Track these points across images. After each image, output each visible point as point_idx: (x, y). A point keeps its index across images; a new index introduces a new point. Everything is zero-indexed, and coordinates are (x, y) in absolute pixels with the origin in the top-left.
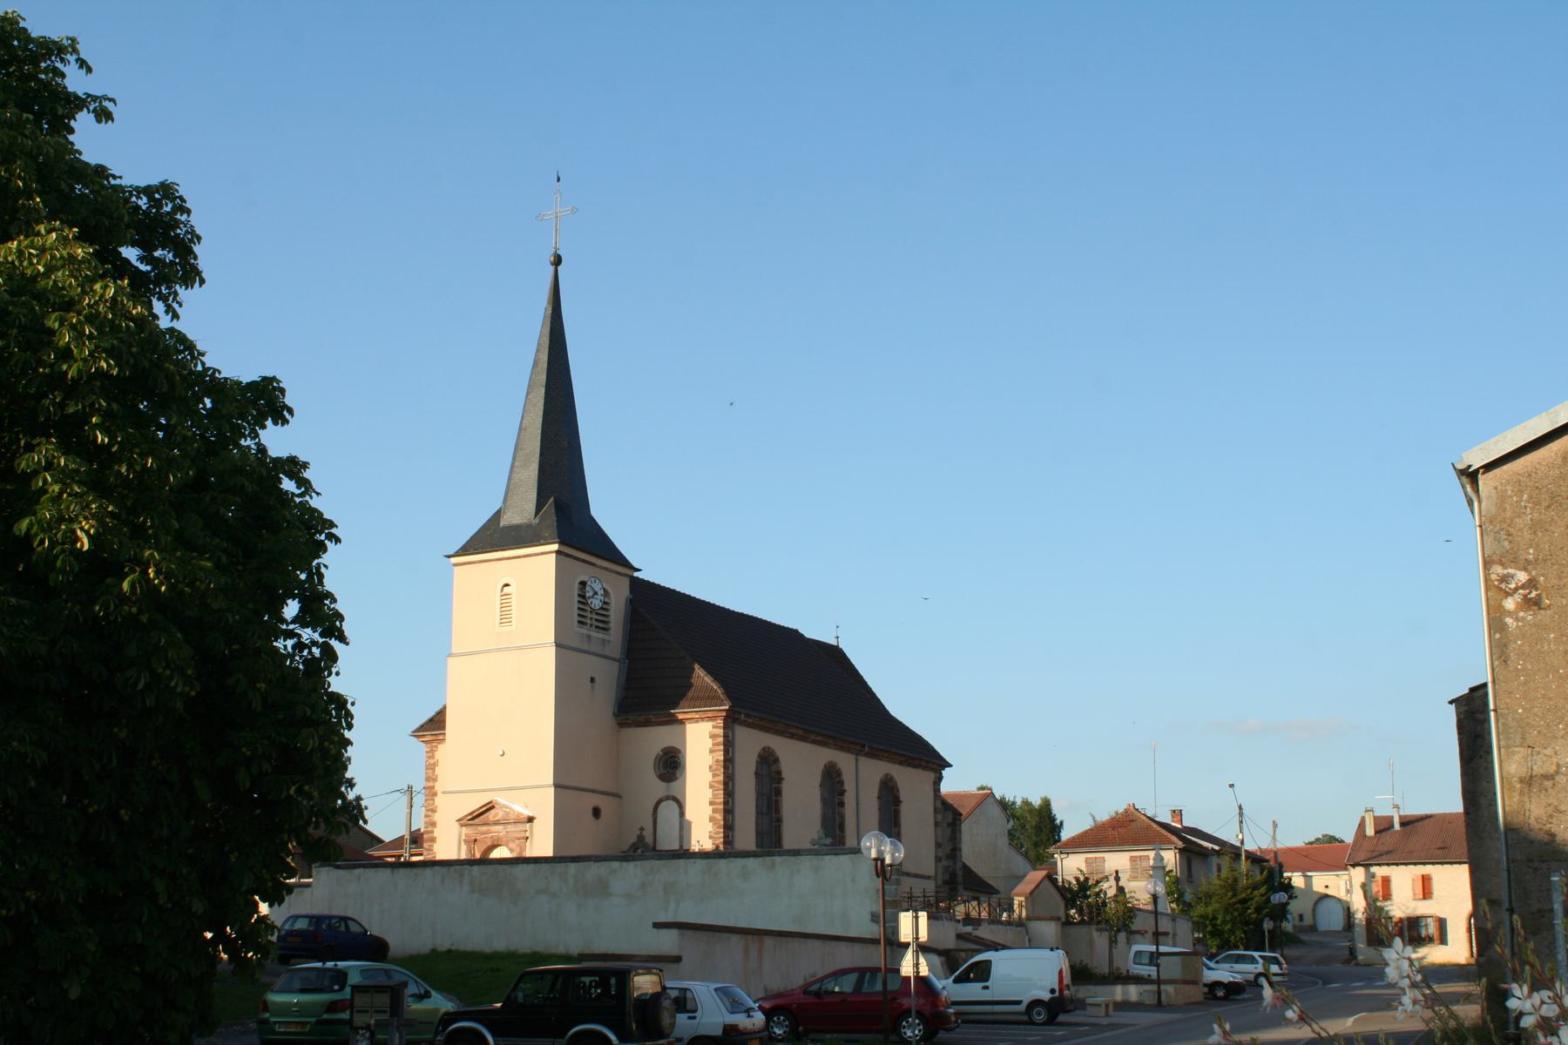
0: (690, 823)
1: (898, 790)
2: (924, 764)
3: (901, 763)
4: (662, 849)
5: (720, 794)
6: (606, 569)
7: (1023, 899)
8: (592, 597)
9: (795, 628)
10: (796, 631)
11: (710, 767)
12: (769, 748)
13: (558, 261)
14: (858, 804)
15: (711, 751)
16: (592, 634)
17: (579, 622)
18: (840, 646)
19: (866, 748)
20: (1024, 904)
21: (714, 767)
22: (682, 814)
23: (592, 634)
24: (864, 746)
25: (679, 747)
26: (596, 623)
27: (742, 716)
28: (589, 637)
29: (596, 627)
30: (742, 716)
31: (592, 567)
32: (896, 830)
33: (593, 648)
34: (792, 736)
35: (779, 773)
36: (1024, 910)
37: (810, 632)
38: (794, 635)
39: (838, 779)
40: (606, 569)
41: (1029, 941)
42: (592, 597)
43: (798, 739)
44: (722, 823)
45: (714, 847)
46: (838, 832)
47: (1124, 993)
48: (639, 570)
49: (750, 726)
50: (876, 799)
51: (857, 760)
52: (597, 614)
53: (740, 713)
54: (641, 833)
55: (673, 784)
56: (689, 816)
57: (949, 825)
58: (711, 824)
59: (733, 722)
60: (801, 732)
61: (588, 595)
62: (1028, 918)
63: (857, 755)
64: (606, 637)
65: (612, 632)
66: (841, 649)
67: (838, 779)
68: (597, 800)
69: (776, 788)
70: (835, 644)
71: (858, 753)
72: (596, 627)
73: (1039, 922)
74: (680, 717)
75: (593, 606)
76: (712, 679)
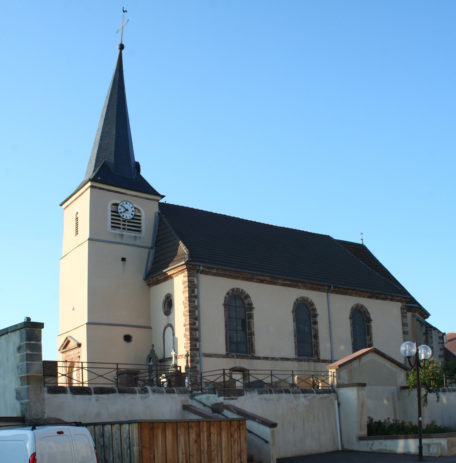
0: (177, 339)
1: (369, 314)
2: (389, 297)
3: (369, 297)
4: (166, 358)
5: (187, 318)
6: (136, 196)
7: (334, 370)
8: (123, 212)
9: (327, 234)
10: (329, 236)
11: (183, 302)
12: (303, 297)
13: (122, 47)
14: (330, 322)
15: (184, 292)
16: (124, 233)
17: (112, 227)
18: (364, 244)
19: (332, 288)
20: (335, 374)
21: (185, 302)
22: (174, 334)
23: (124, 233)
24: (330, 286)
25: (172, 294)
26: (127, 227)
27: (201, 267)
28: (122, 235)
29: (128, 229)
30: (201, 267)
31: (125, 195)
32: (369, 337)
33: (124, 241)
34: (261, 281)
35: (250, 304)
36: (335, 379)
37: (336, 236)
38: (327, 238)
39: (311, 308)
40: (136, 196)
41: (339, 404)
42: (123, 212)
43: (266, 283)
44: (189, 337)
45: (187, 353)
46: (313, 340)
47: (406, 446)
48: (163, 197)
49: (206, 273)
50: (349, 319)
51: (328, 296)
52: (128, 222)
53: (200, 266)
54: (153, 349)
55: (169, 316)
56: (176, 335)
57: (424, 334)
58: (185, 338)
59: (197, 272)
60: (268, 279)
61: (119, 211)
62: (339, 386)
63: (327, 292)
64: (137, 234)
65: (143, 232)
66: (364, 246)
67: (311, 308)
68: (128, 331)
69: (248, 314)
70: (361, 243)
71: (328, 291)
72: (128, 229)
73: (345, 388)
74: (169, 273)
75: (125, 217)
76: (185, 247)
